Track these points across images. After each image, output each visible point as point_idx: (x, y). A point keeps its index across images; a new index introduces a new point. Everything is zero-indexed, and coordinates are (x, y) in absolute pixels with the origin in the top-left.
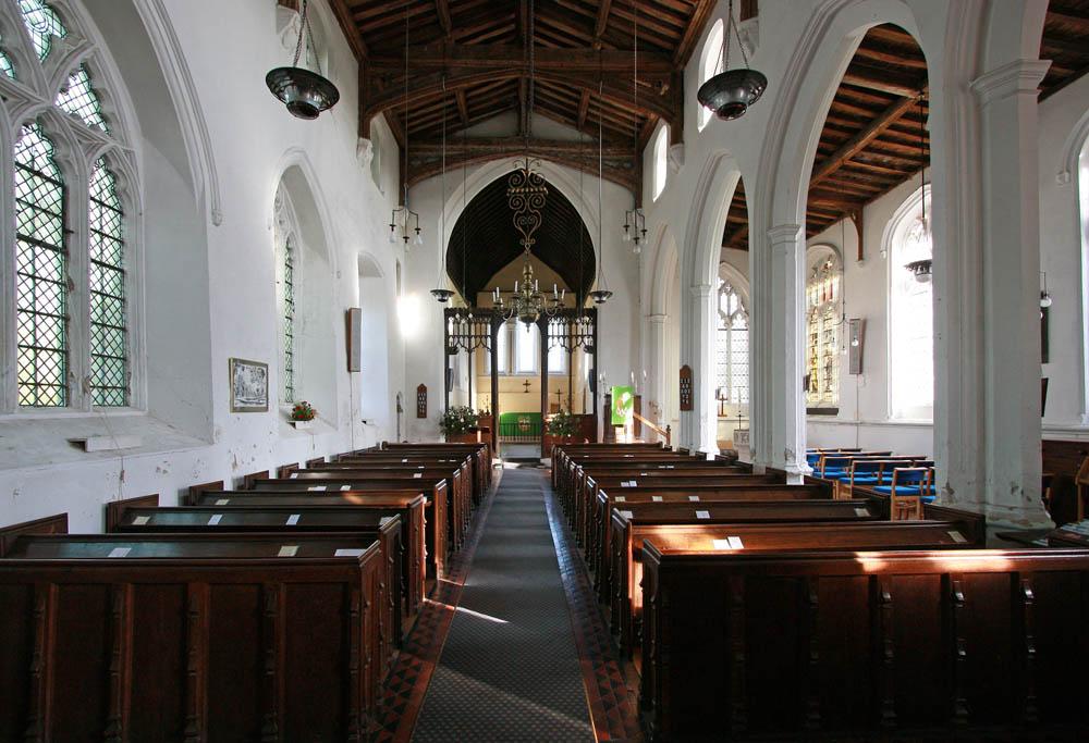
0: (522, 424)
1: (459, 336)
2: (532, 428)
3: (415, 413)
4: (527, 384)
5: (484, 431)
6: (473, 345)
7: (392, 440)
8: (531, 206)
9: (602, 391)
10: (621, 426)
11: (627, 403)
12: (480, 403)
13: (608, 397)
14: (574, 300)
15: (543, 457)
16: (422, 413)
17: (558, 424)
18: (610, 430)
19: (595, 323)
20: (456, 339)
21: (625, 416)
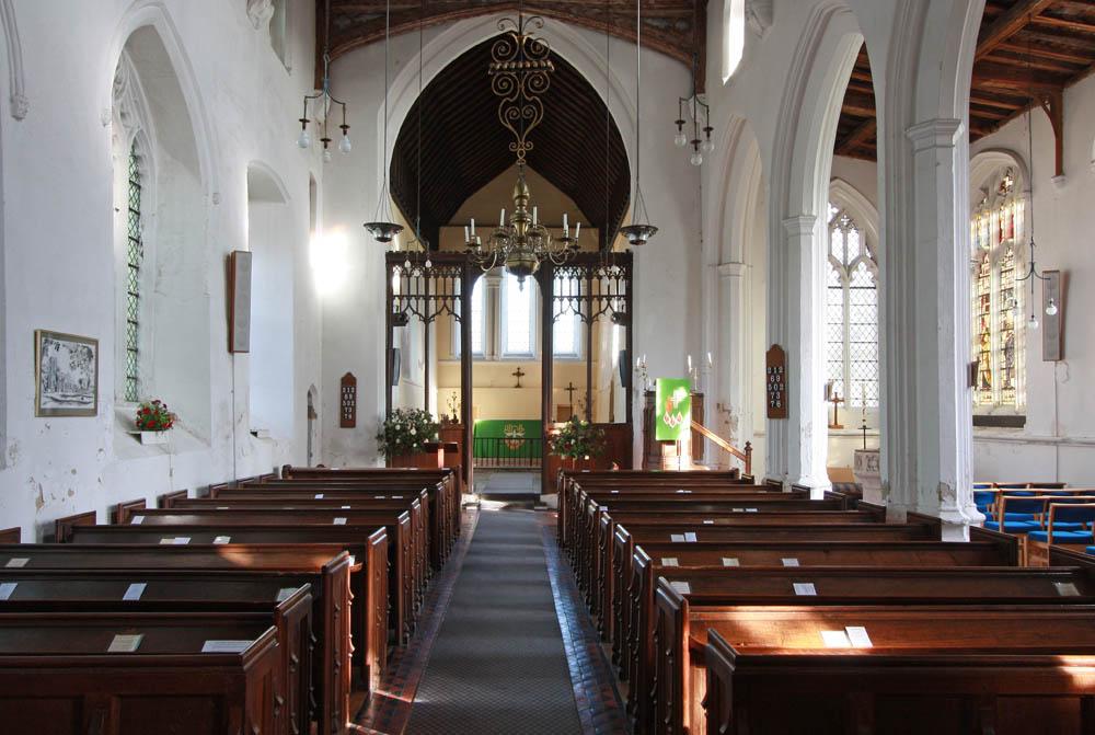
0: (511, 438)
1: (409, 297)
2: (527, 445)
4: (519, 374)
5: (450, 449)
6: (432, 311)
7: (300, 463)
8: (527, 89)
9: (640, 386)
10: (671, 442)
11: (682, 406)
12: (442, 404)
13: (650, 395)
14: (596, 239)
15: (544, 492)
16: (348, 420)
17: (569, 438)
18: (653, 450)
19: (628, 276)
20: (405, 301)
21: (677, 427)
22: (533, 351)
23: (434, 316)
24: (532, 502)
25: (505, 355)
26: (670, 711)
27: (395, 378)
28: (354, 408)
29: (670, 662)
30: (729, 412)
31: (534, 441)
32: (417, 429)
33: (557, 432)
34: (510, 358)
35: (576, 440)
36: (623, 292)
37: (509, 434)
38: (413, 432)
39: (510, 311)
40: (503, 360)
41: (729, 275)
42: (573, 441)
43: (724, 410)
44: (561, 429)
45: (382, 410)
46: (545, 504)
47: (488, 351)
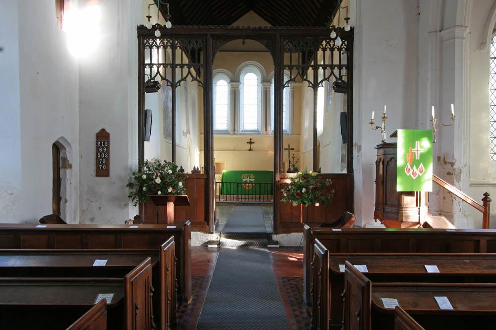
0: (246, 183)
2: (262, 187)
3: (93, 173)
4: (251, 143)
5: (180, 202)
6: (178, 78)
10: (410, 194)
11: (424, 158)
12: (192, 159)
14: (297, 56)
15: (276, 232)
16: (102, 170)
17: (300, 187)
18: (389, 202)
19: (350, 50)
21: (418, 179)
22: (260, 130)
23: (179, 82)
24: (266, 241)
25: (242, 131)
26: (320, 299)
27: (147, 135)
28: (108, 160)
29: (320, 277)
30: (452, 164)
31: (262, 185)
32: (162, 179)
33: (288, 181)
34: (245, 133)
35: (307, 188)
36: (344, 62)
37: (244, 180)
38: (158, 181)
39: (243, 99)
40: (241, 134)
41: (455, 38)
42: (304, 190)
43: (445, 163)
44: (292, 179)
45: (134, 161)
46: (276, 243)
47: (232, 129)
